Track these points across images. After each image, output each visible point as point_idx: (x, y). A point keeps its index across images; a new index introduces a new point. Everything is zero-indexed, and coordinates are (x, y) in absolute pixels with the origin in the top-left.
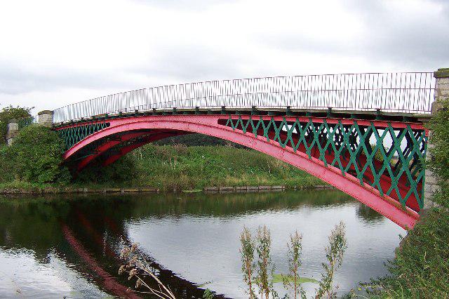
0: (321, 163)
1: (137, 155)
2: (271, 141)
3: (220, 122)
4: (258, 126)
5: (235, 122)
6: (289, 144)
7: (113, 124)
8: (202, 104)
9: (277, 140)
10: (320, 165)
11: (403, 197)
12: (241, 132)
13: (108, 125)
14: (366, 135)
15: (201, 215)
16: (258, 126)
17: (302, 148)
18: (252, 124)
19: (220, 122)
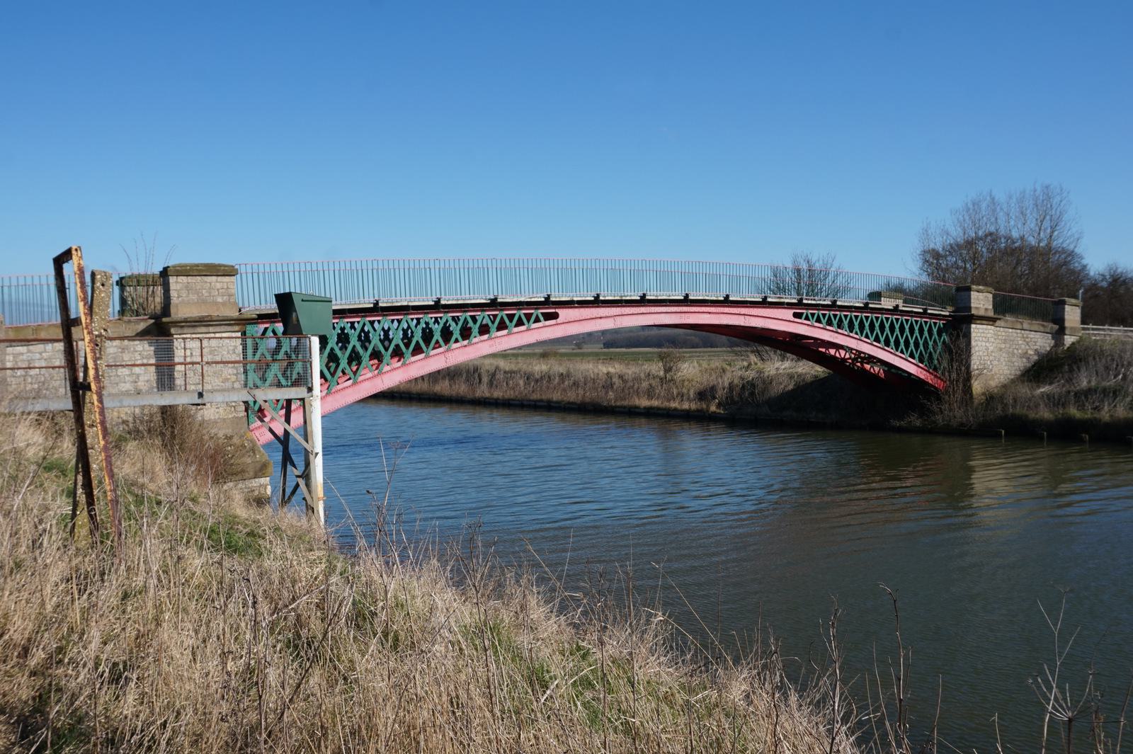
3: (796, 315)
7: (564, 314)
12: (821, 326)
19: (796, 315)
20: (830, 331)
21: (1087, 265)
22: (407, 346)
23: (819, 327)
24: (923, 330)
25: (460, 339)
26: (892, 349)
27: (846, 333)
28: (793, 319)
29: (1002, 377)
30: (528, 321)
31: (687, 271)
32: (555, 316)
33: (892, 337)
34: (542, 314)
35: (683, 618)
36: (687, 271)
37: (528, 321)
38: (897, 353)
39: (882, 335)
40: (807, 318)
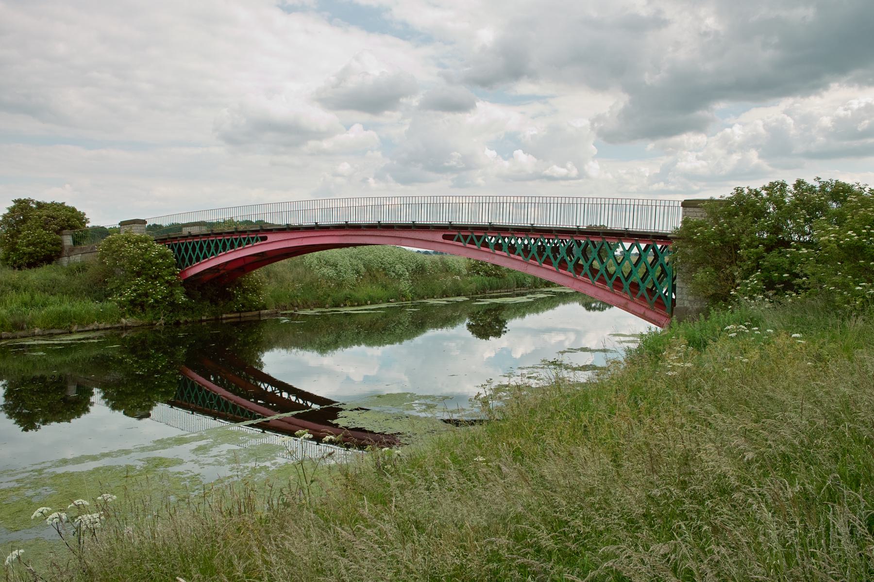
0: (570, 274)
1: (258, 274)
2: (512, 256)
3: (445, 237)
4: (177, 246)
5: (466, 237)
6: (533, 258)
7: (271, 237)
8: (423, 219)
9: (519, 255)
10: (570, 277)
11: (540, 260)
12: (475, 247)
13: (265, 238)
14: (582, 247)
15: (327, 399)
16: (177, 246)
17: (548, 262)
18: (203, 242)
19: (445, 237)
20: (498, 255)
21: (15, 424)
22: (209, 253)
23: (487, 252)
24: (210, 247)
25: (222, 251)
26: (570, 272)
27: (505, 254)
28: (442, 240)
29: (257, 361)
30: (253, 240)
31: (376, 204)
32: (265, 238)
33: (194, 255)
34: (260, 237)
35: (258, 350)
36: (376, 204)
37: (253, 240)
38: (581, 277)
39: (201, 254)
40: (459, 240)
